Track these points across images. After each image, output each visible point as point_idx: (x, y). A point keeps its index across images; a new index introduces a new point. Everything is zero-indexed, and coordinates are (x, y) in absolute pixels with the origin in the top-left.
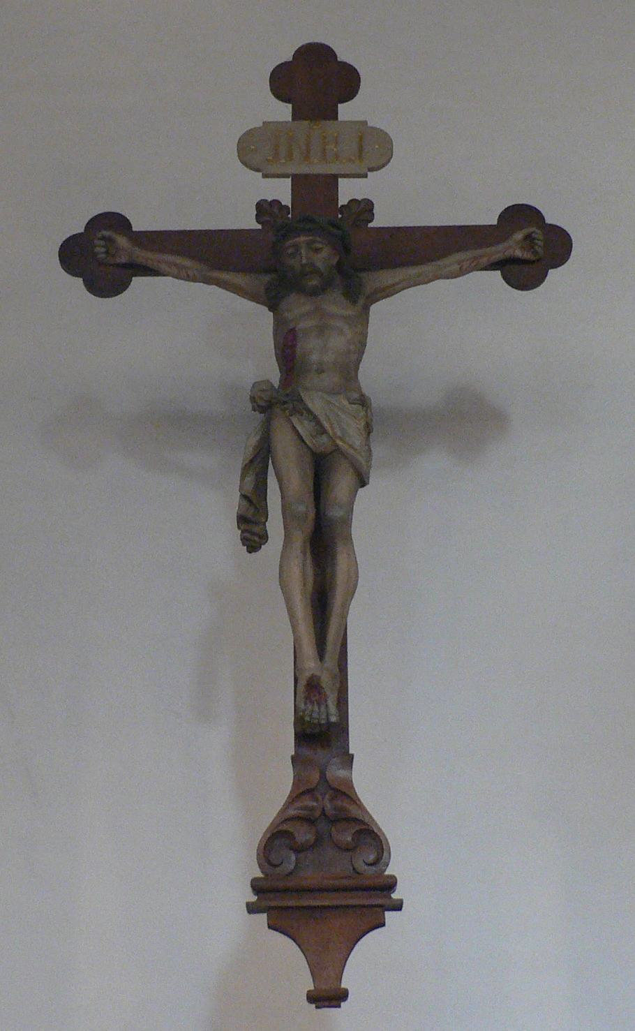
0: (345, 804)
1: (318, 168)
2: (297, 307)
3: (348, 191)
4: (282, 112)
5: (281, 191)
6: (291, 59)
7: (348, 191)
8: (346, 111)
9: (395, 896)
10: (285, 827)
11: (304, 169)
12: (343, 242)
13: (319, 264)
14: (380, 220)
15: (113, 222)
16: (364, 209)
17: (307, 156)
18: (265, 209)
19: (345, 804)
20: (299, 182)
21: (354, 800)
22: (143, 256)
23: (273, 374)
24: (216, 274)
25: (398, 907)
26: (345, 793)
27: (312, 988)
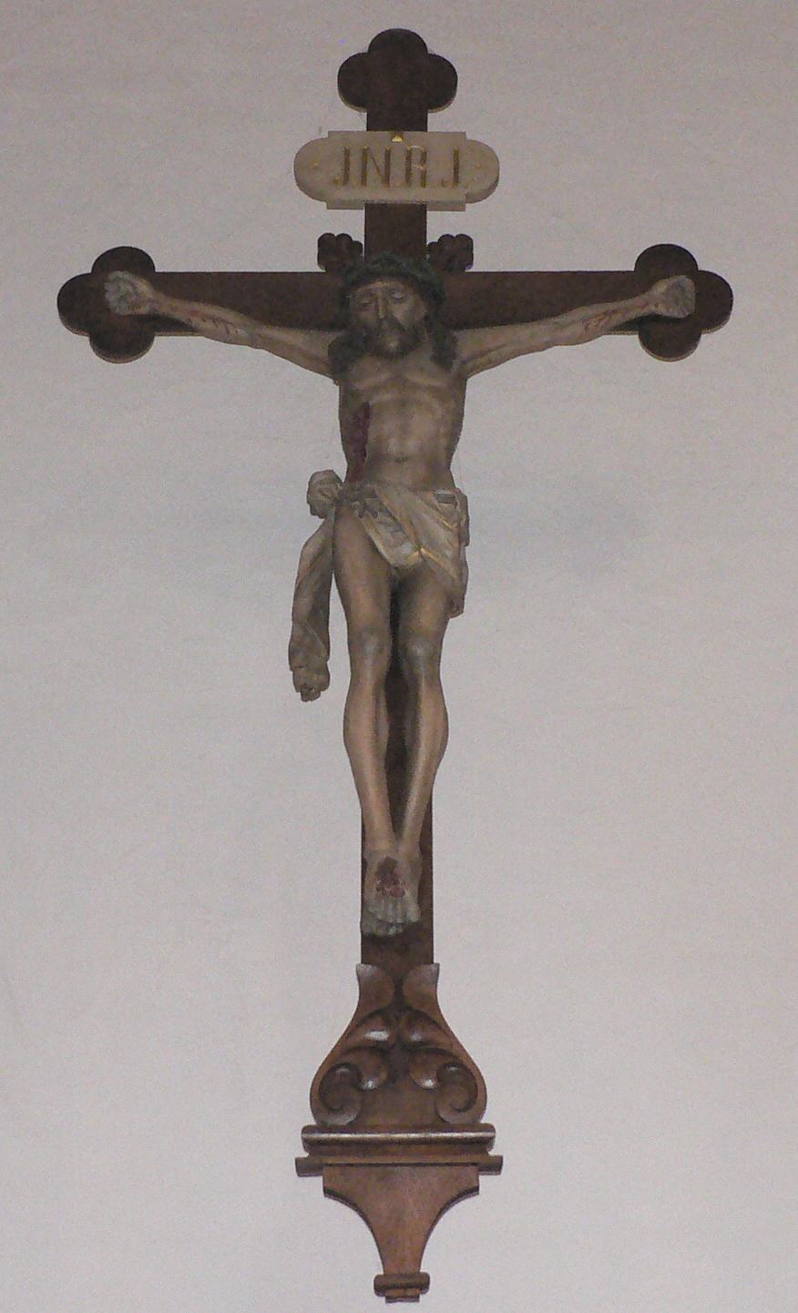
1: (399, 194)
2: (372, 375)
3: (438, 226)
5: (353, 225)
7: (438, 226)
8: (438, 121)
14: (483, 262)
15: (130, 260)
16: (461, 246)
18: (330, 246)
20: (376, 215)
21: (440, 1025)
25: (495, 1166)
26: (428, 1015)
27: (382, 1273)
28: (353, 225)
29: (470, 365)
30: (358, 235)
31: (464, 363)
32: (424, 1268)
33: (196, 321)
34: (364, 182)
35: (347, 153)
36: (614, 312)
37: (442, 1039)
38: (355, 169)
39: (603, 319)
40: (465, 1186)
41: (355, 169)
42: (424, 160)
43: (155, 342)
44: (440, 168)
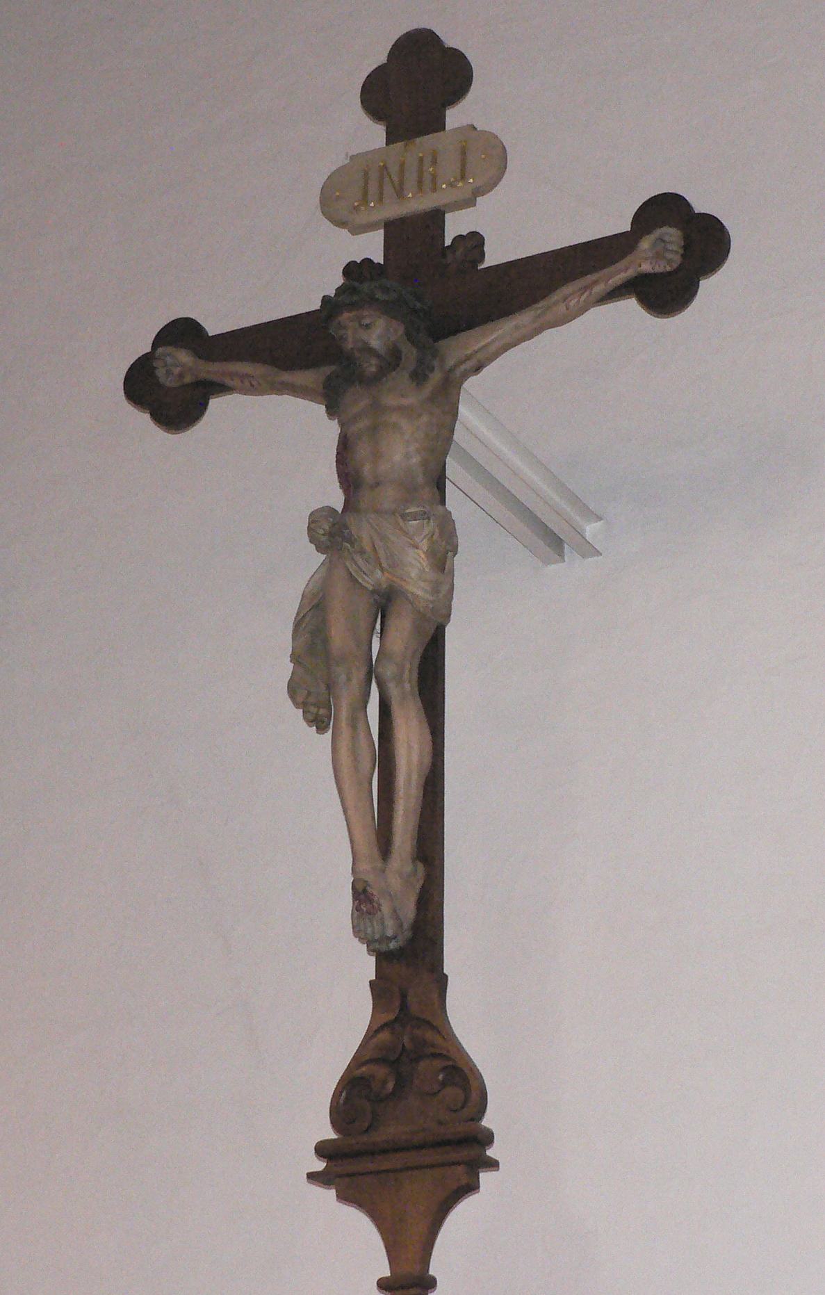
0: (429, 1035)
1: (417, 204)
2: (357, 401)
3: (455, 226)
4: (375, 135)
5: (372, 247)
6: (386, 62)
7: (455, 226)
8: (455, 117)
9: (490, 1153)
10: (358, 1072)
11: (393, 210)
12: (169, 355)
13: (375, 343)
14: (494, 256)
16: (474, 242)
17: (400, 193)
19: (429, 1035)
20: (395, 231)
22: (211, 370)
23: (336, 499)
24: (286, 377)
25: (493, 1165)
27: (388, 1274)
28: (372, 247)
29: (458, 372)
30: (379, 258)
31: (452, 370)
32: (431, 1272)
33: (228, 382)
34: (381, 199)
35: (366, 174)
36: (595, 283)
37: (438, 1040)
38: (373, 189)
39: (583, 293)
40: (464, 1181)
41: (373, 189)
42: (434, 162)
43: (210, 404)
44: (449, 167)
